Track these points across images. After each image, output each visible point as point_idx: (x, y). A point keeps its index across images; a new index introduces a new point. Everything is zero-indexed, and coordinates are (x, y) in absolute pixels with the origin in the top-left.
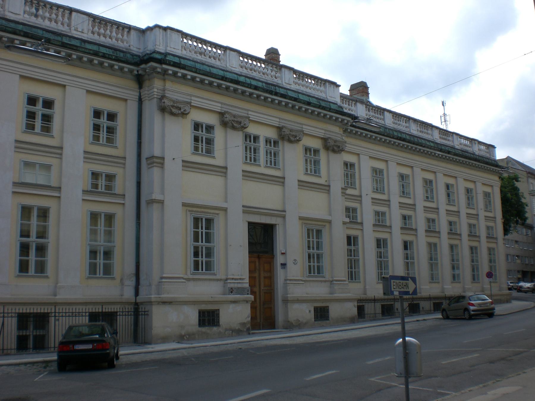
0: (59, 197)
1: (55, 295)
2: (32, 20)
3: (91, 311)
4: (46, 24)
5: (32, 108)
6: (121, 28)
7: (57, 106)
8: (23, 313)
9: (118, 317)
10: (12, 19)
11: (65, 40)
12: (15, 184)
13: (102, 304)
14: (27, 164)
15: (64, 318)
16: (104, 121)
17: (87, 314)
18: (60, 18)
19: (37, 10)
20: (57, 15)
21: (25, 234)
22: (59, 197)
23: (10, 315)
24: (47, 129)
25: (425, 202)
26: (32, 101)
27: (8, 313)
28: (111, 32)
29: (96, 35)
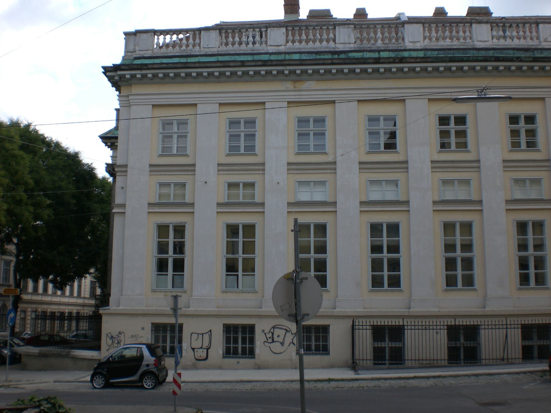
0: (482, 210)
1: (485, 308)
2: (502, 43)
3: (523, 323)
4: (516, 43)
5: (515, 127)
6: (521, 25)
7: (539, 120)
8: (466, 325)
9: (406, 331)
10: (482, 47)
11: (538, 55)
12: (508, 202)
13: (455, 317)
14: (445, 182)
15: (487, 330)
16: (452, 127)
17: (520, 326)
18: (528, 33)
19: (504, 31)
20: (524, 32)
21: (522, 247)
22: (482, 210)
23: (513, 326)
24: (463, 146)
25: (511, 153)
26: (514, 119)
27: (511, 325)
28: (524, 32)
29: (448, 40)
